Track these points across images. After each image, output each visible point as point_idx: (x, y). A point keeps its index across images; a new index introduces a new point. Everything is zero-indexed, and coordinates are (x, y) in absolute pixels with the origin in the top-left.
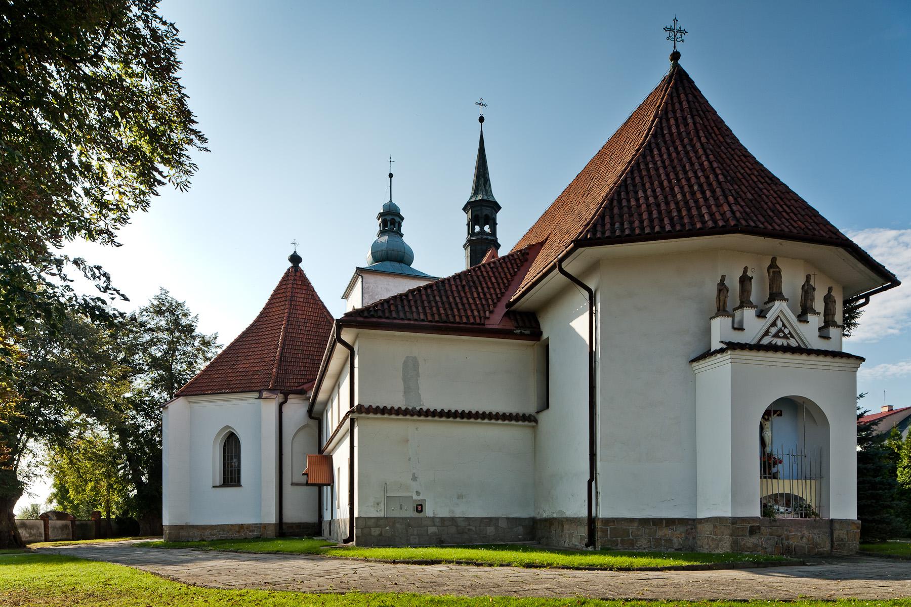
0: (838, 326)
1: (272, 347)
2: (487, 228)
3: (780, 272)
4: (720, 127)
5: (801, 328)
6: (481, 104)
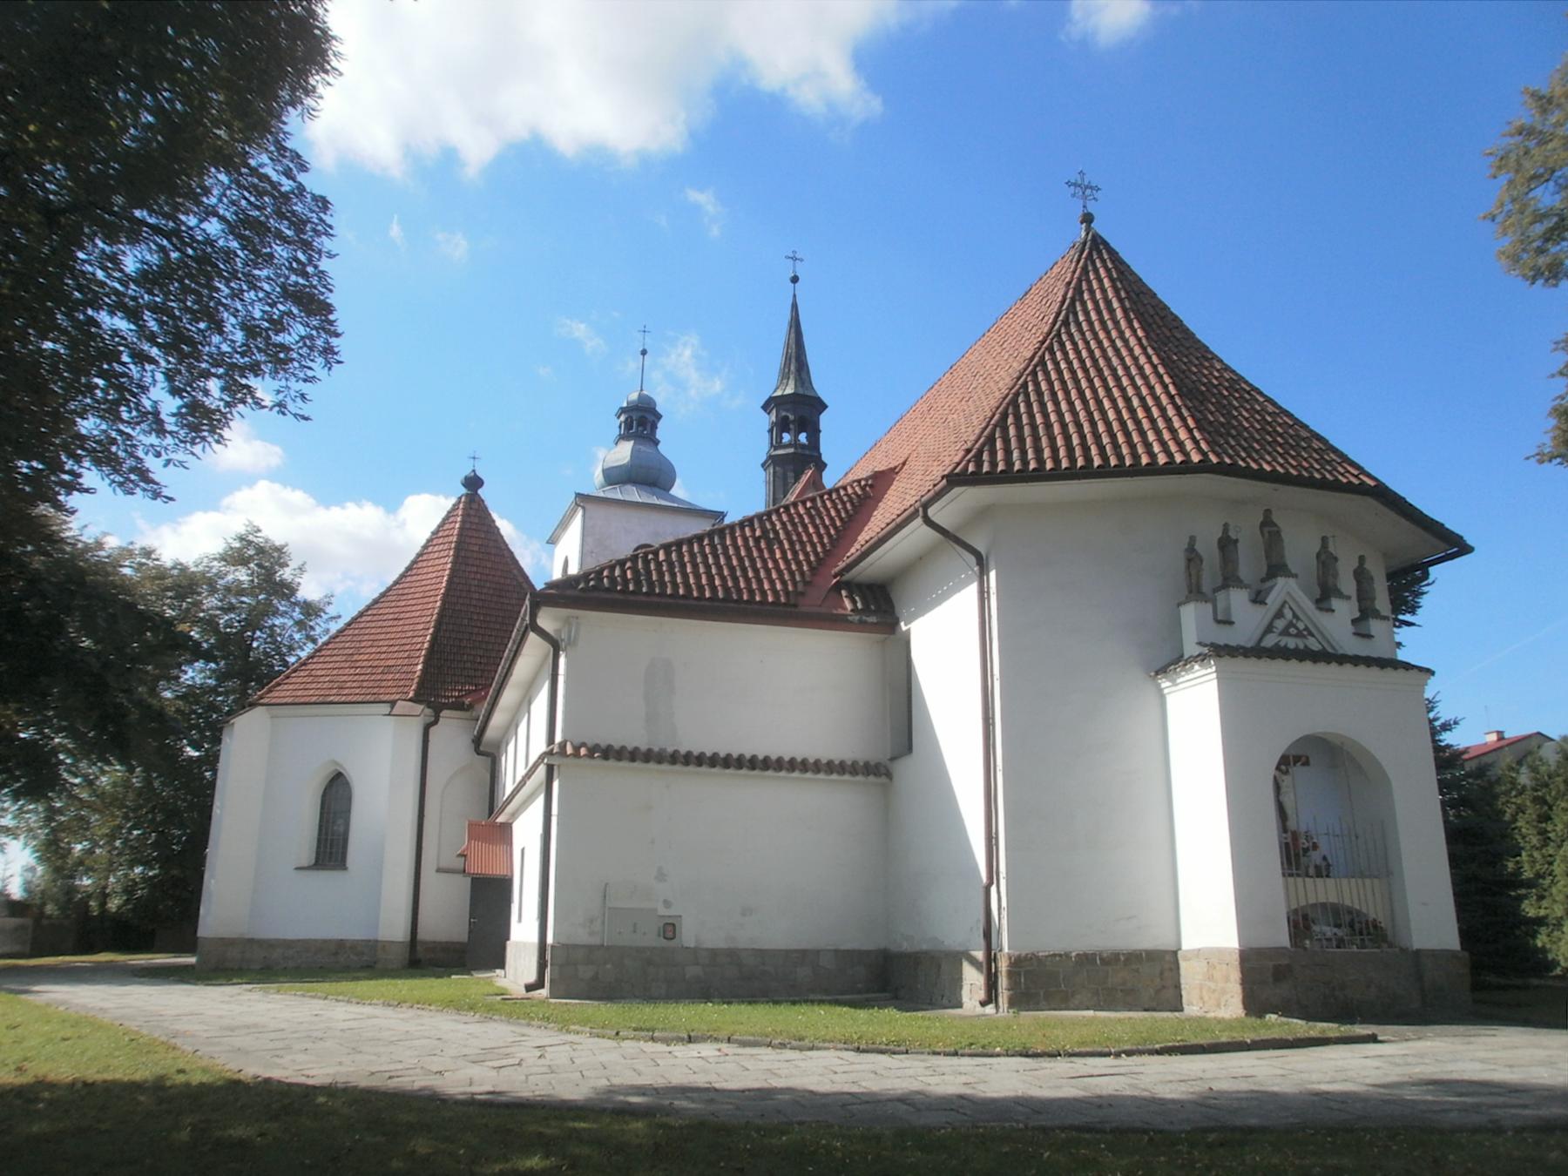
0: (1385, 618)
1: (421, 627)
2: (803, 437)
3: (1278, 533)
4: (1162, 315)
5: (1323, 620)
6: (795, 259)
